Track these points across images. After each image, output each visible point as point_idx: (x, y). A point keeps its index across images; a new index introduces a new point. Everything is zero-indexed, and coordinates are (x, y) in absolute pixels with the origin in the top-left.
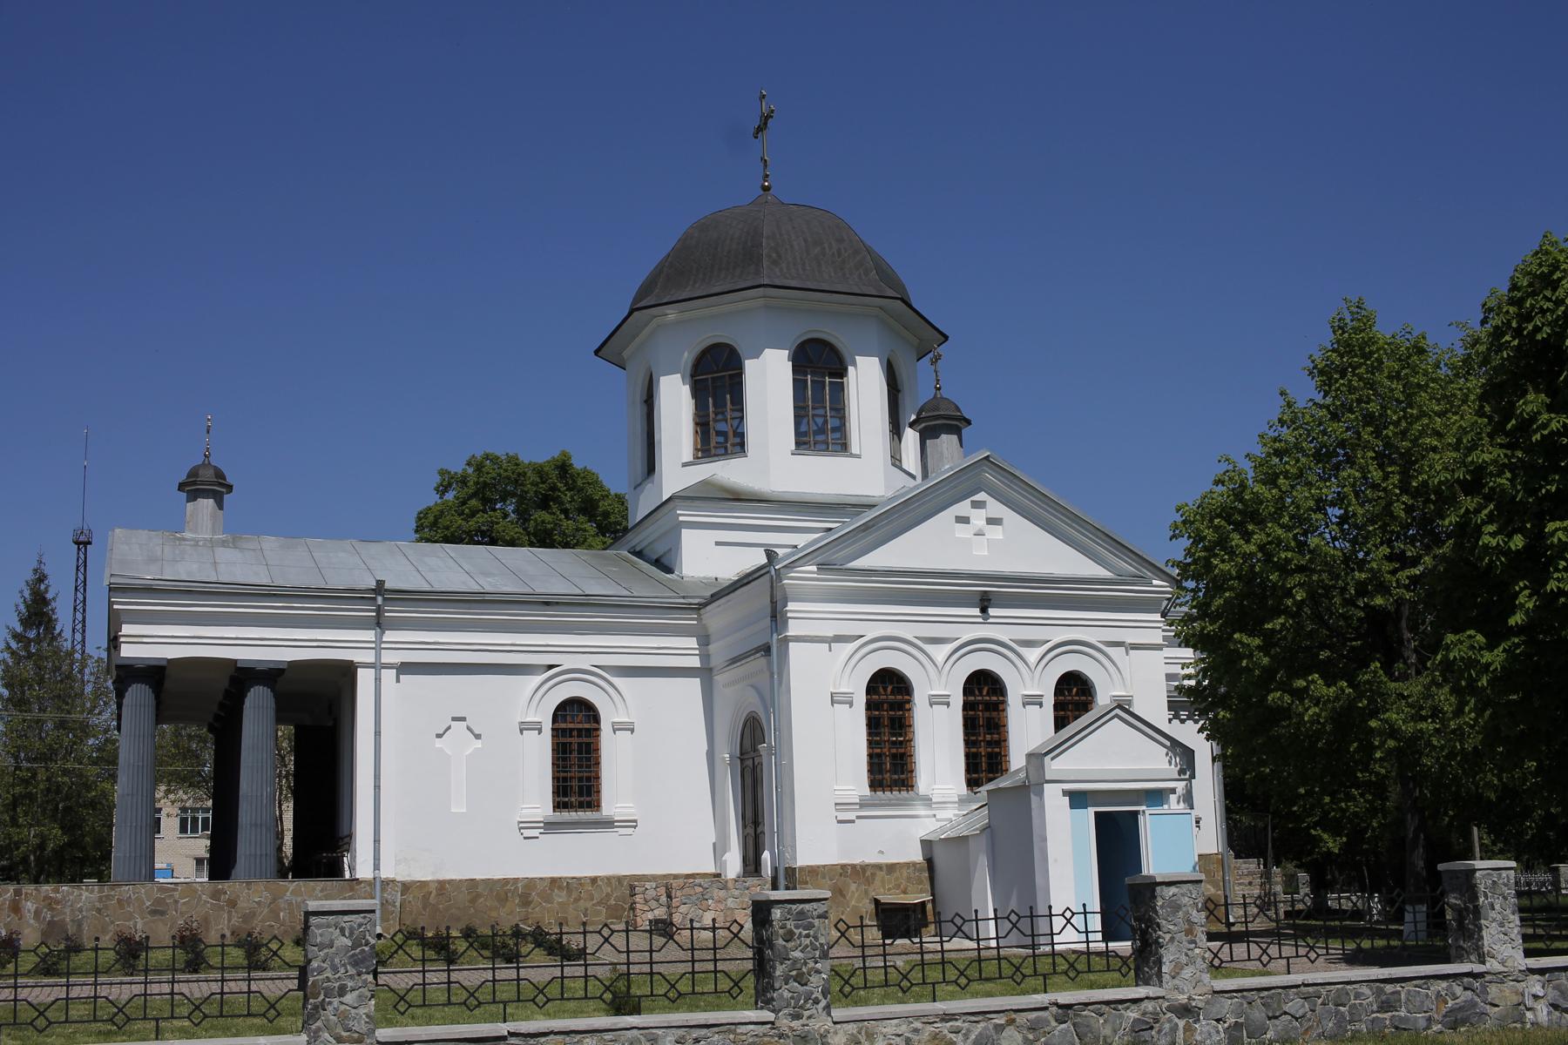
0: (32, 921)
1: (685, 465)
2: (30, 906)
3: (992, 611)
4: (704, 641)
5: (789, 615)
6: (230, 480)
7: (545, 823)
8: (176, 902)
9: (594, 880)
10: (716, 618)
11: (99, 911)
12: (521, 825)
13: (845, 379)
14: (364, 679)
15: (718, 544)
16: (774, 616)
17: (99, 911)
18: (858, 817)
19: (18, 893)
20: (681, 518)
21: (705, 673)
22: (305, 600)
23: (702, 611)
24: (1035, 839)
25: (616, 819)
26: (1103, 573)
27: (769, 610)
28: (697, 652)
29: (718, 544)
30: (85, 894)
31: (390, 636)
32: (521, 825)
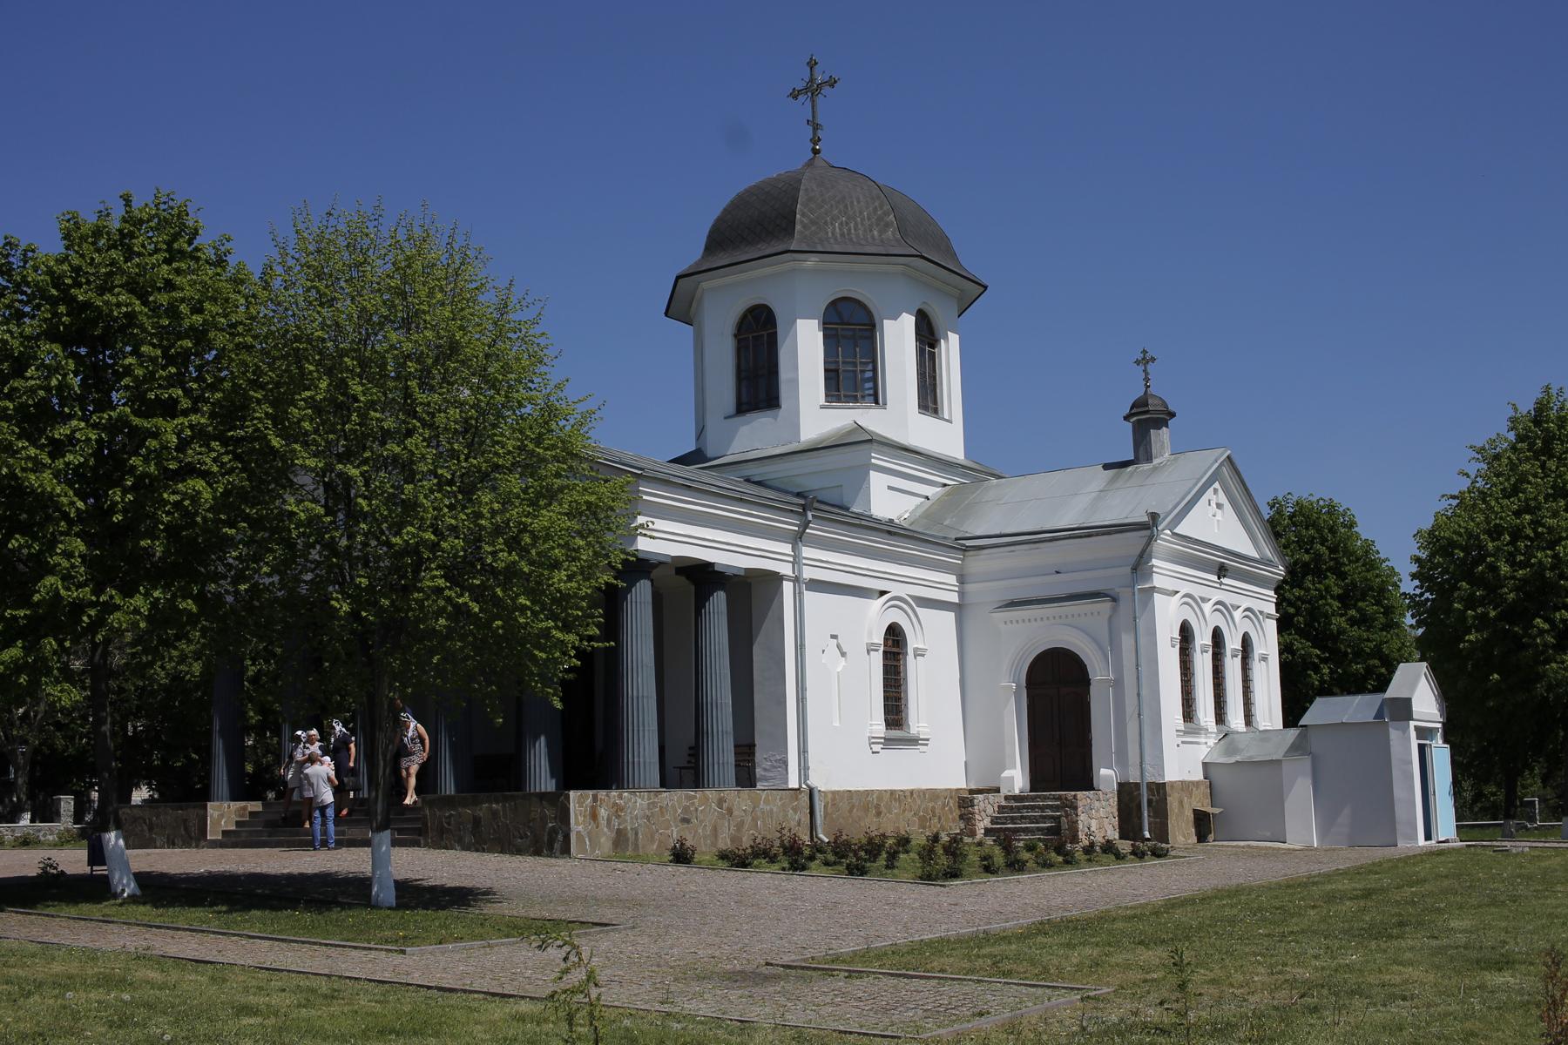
0: (605, 829)
1: (822, 407)
2: (603, 813)
3: (1225, 580)
4: (962, 580)
5: (1154, 569)
6: (1171, 408)
7: (885, 738)
8: (697, 810)
9: (912, 792)
10: (978, 564)
11: (648, 818)
12: (873, 740)
13: (936, 350)
14: (788, 587)
15: (890, 488)
16: (1135, 569)
17: (648, 818)
18: (1183, 742)
19: (595, 798)
20: (873, 461)
21: (958, 609)
22: (764, 509)
23: (967, 554)
24: (1396, 773)
25: (921, 737)
26: (1254, 554)
27: (1133, 561)
28: (957, 589)
29: (890, 488)
30: (639, 800)
31: (807, 552)
32: (873, 740)
